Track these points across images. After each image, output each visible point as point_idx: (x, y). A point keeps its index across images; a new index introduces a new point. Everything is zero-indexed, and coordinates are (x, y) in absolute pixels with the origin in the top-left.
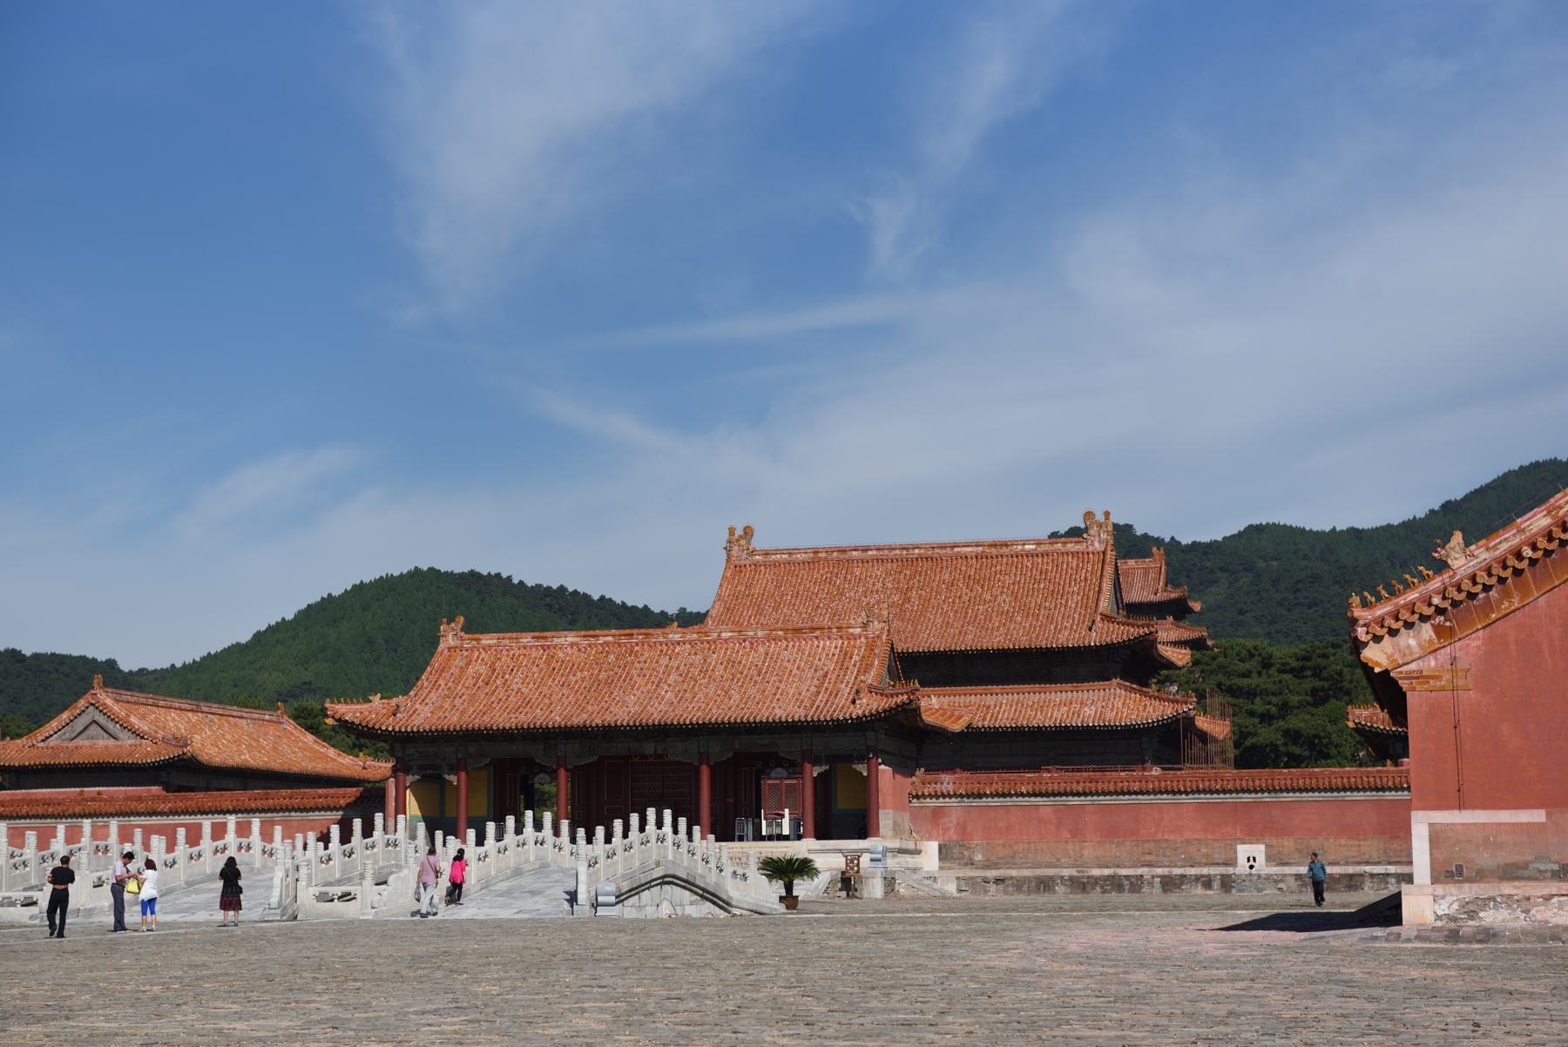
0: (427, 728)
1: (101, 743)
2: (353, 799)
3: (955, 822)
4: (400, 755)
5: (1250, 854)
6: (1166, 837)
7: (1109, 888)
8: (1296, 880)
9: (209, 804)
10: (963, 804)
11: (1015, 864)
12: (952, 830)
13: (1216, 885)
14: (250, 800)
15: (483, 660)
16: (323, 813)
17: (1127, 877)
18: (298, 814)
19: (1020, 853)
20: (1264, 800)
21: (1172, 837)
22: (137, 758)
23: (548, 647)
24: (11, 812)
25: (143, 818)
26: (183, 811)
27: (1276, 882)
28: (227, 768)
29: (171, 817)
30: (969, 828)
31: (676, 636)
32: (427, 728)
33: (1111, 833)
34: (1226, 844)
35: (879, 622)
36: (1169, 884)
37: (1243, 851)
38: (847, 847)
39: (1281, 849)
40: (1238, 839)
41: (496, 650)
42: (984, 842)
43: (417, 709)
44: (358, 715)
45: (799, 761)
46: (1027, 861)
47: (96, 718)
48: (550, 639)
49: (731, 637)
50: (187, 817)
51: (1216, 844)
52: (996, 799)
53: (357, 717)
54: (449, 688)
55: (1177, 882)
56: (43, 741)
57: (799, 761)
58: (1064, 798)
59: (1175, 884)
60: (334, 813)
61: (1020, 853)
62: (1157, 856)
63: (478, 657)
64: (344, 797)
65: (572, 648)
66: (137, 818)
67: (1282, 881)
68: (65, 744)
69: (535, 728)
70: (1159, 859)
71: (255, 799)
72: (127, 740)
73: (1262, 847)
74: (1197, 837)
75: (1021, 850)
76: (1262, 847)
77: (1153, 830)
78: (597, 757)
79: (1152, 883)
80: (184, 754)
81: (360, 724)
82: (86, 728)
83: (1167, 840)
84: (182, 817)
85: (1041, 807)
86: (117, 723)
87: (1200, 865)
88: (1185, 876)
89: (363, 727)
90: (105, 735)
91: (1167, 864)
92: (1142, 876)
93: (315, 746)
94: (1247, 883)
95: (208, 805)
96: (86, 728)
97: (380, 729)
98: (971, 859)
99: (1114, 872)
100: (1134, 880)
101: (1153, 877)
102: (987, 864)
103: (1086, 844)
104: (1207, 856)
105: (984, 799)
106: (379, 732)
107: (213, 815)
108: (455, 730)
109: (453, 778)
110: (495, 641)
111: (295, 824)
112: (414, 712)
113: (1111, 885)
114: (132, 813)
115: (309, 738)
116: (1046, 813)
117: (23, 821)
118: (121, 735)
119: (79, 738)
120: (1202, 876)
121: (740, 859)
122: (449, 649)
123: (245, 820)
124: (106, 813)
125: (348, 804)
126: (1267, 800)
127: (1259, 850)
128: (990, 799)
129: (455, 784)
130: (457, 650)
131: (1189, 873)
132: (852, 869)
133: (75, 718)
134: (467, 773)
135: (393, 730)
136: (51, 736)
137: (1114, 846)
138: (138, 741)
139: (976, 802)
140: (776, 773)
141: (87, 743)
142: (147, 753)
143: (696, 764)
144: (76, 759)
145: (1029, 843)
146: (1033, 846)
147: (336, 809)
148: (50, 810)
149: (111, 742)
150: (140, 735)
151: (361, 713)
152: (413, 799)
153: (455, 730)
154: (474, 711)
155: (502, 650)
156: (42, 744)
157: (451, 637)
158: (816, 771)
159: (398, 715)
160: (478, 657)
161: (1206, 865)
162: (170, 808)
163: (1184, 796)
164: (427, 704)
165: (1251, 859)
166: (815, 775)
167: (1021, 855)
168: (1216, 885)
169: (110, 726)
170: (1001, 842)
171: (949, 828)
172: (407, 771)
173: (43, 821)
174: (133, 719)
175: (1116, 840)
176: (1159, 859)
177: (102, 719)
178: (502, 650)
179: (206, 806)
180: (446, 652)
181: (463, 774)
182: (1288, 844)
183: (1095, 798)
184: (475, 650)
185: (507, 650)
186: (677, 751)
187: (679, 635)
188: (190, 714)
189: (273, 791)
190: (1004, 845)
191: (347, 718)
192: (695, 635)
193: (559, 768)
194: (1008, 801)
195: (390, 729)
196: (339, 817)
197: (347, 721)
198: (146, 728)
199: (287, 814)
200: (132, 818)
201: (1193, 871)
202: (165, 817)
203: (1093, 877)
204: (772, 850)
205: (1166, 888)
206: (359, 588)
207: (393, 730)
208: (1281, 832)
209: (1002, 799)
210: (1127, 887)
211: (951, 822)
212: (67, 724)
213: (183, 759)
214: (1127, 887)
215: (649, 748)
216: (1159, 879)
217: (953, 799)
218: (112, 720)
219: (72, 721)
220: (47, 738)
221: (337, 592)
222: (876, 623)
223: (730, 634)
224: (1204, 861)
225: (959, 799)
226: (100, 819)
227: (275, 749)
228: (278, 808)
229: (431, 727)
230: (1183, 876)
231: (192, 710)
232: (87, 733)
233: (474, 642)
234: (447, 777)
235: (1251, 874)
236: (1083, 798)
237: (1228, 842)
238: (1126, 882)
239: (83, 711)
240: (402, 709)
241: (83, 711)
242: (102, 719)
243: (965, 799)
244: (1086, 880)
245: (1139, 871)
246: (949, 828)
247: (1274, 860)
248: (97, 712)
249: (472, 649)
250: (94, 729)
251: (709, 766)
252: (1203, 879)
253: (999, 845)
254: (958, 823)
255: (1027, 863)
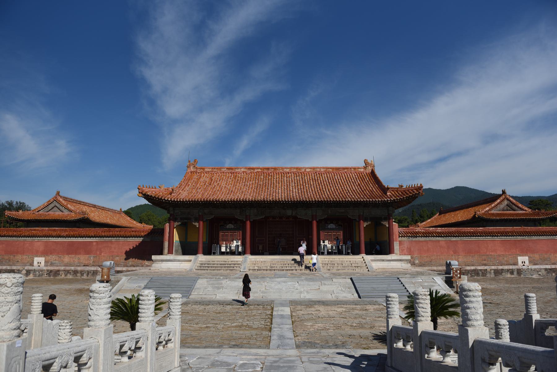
0: (187, 200)
1: (57, 213)
2: (147, 233)
3: (406, 247)
4: (172, 213)
5: (523, 261)
6: (491, 254)
7: (473, 274)
8: (545, 271)
9: (84, 233)
10: (409, 240)
11: (432, 264)
12: (405, 250)
13: (515, 273)
14: (102, 232)
15: (206, 176)
16: (134, 238)
17: (481, 270)
18: (123, 238)
19: (434, 260)
20: (526, 239)
21: (493, 254)
22: (69, 218)
23: (233, 173)
24: (76, 234)
25: (55, 238)
26: (67, 236)
27: (538, 272)
28: (101, 223)
29: (67, 238)
30: (412, 249)
31: (287, 170)
32: (187, 200)
33: (469, 252)
34: (514, 257)
35: (371, 167)
36: (498, 272)
37: (520, 259)
38: (386, 259)
39: (534, 258)
40: (518, 254)
41: (211, 173)
42: (419, 255)
43: (181, 193)
44: (154, 193)
45: (358, 220)
46: (436, 263)
47: (56, 205)
48: (234, 170)
49: (310, 171)
50: (74, 238)
51: (510, 256)
52: (423, 238)
53: (154, 194)
54: (194, 186)
55: (500, 272)
56: (37, 212)
57: (358, 220)
58: (450, 238)
59: (499, 273)
60: (139, 238)
61: (434, 260)
62: (488, 261)
63: (204, 175)
64: (143, 232)
65: (244, 173)
66: (52, 238)
67: (540, 271)
68: (45, 213)
69: (240, 201)
70: (489, 262)
71: (104, 232)
72: (66, 212)
73: (527, 258)
74: (502, 253)
75: (434, 259)
76: (527, 258)
77: (485, 251)
78: (264, 216)
79: (491, 273)
80: (84, 217)
81: (155, 197)
82: (53, 208)
83: (491, 255)
84: (72, 238)
85: (441, 242)
86: (63, 207)
87: (505, 265)
88: (503, 269)
89: (156, 198)
90: (59, 211)
91: (492, 264)
92: (486, 270)
93: (130, 220)
94: (527, 272)
95: (40, 233)
96: (53, 208)
97: (164, 199)
98: (414, 262)
99: (476, 268)
100: (483, 271)
101: (491, 270)
102: (420, 264)
103: (460, 256)
104: (507, 261)
105: (418, 238)
106: (164, 201)
107: (85, 238)
108: (201, 201)
109: (197, 224)
110: (211, 170)
111: (121, 243)
112: (180, 194)
113: (474, 273)
114: (50, 236)
115: (129, 218)
116: (443, 244)
117: (3, 238)
118: (64, 211)
119: (50, 211)
120: (510, 269)
121: (342, 264)
122: (191, 172)
123: (99, 240)
124: (50, 236)
125: (145, 235)
126: (527, 239)
127: (526, 259)
128: (420, 238)
129: (198, 226)
130: (195, 173)
131: (504, 268)
132: (457, 276)
133: (49, 204)
134: (203, 222)
135: (171, 200)
136: (40, 210)
137: (471, 257)
138: (70, 213)
139: (414, 239)
140: (331, 226)
141: (52, 213)
142: (73, 217)
143: (310, 220)
144: (47, 218)
145: (437, 256)
146: (439, 257)
147: (142, 237)
148: (15, 234)
149: (61, 213)
150: (70, 211)
151: (155, 192)
152: (177, 233)
153: (201, 201)
154: (208, 194)
155: (214, 173)
156: (37, 213)
157: (192, 167)
158: (365, 224)
159: (173, 194)
160: (204, 175)
161: (507, 265)
162: (67, 234)
163: (496, 237)
164: (185, 191)
165: (523, 262)
166: (365, 226)
167: (434, 261)
168: (515, 273)
169: (61, 208)
170: (426, 255)
171: (404, 250)
172: (175, 220)
173: (12, 238)
174: (69, 206)
175: (471, 255)
176: (489, 262)
177: (58, 205)
178: (214, 173)
179: (82, 234)
180: (190, 173)
181: (201, 223)
182: (537, 256)
183: (462, 238)
184: (202, 173)
185: (216, 173)
186: (303, 214)
187: (289, 170)
188: (92, 208)
189: (113, 229)
190: (427, 257)
191: (149, 194)
192: (295, 170)
193: (247, 220)
194: (427, 239)
195: (169, 199)
196: (141, 240)
197: (148, 195)
198: (73, 209)
199: (118, 238)
200: (50, 238)
201: (506, 267)
202: (64, 238)
203: (467, 270)
204: (355, 260)
205: (496, 274)
206: (137, 206)
207: (171, 200)
208: (533, 252)
209: (425, 238)
210: (481, 274)
211: (404, 247)
212: (46, 207)
213: (84, 219)
214: (481, 274)
215: (289, 212)
216: (493, 271)
217: (405, 238)
218: (62, 206)
219: (48, 206)
220: (39, 211)
221: (133, 207)
222: (369, 167)
223: (310, 170)
224: (506, 263)
225: (408, 238)
226: (36, 238)
227: (118, 220)
228: (114, 236)
229: (189, 199)
230: (502, 270)
231: (93, 207)
232: (53, 210)
233: (202, 170)
234: (194, 223)
235: (528, 269)
236: (457, 238)
237: (514, 256)
238: (480, 272)
239: (52, 203)
240: (175, 192)
241: (52, 203)
242: (58, 205)
243: (410, 238)
244: (464, 271)
245: (486, 268)
246: (404, 250)
247: (532, 263)
248: (57, 203)
249: (201, 173)
250: (55, 209)
251: (316, 221)
252: (510, 271)
253: (425, 257)
254: (407, 248)
255: (436, 264)
